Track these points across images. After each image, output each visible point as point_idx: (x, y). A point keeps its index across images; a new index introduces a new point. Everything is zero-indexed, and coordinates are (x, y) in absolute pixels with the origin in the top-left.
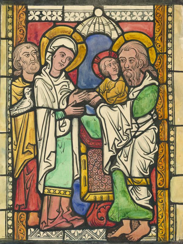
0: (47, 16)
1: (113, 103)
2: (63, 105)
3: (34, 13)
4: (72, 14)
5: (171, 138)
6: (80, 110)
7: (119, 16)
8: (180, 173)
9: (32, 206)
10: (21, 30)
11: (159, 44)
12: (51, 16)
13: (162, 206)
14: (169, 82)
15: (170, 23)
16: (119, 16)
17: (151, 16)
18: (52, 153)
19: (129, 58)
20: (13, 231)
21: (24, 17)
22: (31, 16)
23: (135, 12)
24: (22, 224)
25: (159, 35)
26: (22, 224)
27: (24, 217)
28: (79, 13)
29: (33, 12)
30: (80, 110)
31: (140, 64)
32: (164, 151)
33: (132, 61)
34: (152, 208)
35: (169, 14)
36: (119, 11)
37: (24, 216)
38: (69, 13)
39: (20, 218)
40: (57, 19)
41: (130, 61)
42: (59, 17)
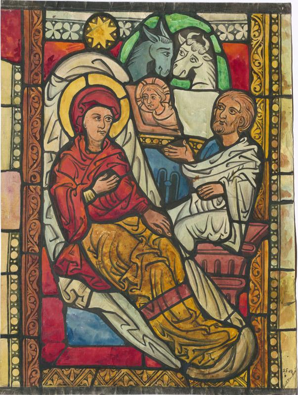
1: (237, 371)
3: (70, 25)
4: (59, 26)
5: (130, 27)
7: (238, 31)
9: (253, 173)
11: (258, 61)
13: (260, 71)
15: (18, 94)
17: (49, 30)
20: (271, 215)
22: (69, 26)
24: (257, 75)
25: (33, 116)
26: (257, 75)
27: (254, 33)
28: (54, 23)
29: (68, 24)
31: (29, 308)
34: (138, 32)
35: (273, 70)
37: (255, 88)
38: (54, 23)
39: (261, 30)
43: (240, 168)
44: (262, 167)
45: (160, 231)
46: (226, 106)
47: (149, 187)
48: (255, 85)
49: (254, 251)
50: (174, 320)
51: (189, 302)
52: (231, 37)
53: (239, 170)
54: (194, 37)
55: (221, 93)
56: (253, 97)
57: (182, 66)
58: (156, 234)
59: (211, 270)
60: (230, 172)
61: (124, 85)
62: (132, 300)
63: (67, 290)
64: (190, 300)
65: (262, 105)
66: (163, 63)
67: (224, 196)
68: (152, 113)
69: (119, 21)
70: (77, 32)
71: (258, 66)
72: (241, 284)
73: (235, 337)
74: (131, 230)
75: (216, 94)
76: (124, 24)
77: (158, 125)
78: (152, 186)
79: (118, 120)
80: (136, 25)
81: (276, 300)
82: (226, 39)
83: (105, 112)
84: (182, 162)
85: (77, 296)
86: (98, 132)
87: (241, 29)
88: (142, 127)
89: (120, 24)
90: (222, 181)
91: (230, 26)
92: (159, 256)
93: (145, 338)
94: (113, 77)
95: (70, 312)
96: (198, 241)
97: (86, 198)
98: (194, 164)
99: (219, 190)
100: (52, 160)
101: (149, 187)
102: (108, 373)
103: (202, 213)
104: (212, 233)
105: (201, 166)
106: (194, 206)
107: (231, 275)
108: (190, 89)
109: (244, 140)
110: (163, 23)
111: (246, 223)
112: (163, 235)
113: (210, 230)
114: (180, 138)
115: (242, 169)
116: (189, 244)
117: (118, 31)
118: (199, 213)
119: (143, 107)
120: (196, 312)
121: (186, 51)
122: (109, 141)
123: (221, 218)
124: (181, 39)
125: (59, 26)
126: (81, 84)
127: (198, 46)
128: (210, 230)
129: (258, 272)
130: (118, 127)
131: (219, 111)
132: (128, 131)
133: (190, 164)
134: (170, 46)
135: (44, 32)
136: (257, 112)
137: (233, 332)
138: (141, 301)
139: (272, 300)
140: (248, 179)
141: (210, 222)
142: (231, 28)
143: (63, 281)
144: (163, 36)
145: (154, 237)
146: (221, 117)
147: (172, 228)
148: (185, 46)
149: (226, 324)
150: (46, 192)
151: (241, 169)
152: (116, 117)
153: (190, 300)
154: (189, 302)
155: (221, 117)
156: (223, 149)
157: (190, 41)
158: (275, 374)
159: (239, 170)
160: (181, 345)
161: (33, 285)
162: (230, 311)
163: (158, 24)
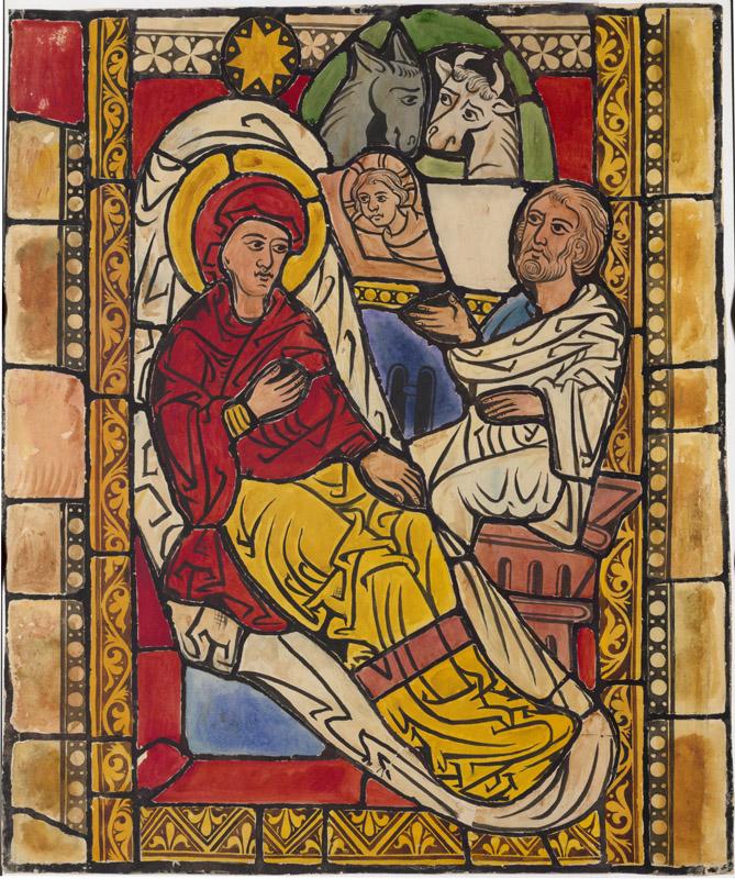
0: (192, 55)
2: (377, 413)
6: (293, 385)
7: (567, 50)
8: (683, 714)
10: (622, 127)
12: (558, 52)
14: (655, 324)
16: (567, 50)
17: (142, 53)
18: (148, 489)
19: (554, 220)
21: (123, 62)
23: (145, 38)
28: (542, 39)
30: (293, 385)
32: (104, 378)
33: (562, 231)
36: (210, 38)
40: (190, 69)
41: (558, 227)
42: (550, 56)
43: (579, 358)
44: (625, 350)
45: (400, 498)
46: (544, 215)
47: (373, 407)
48: (609, 168)
49: (604, 547)
50: (431, 697)
51: (467, 658)
52: (553, 63)
53: (574, 364)
54: (469, 65)
55: (533, 190)
56: (606, 201)
57: (449, 126)
58: (391, 501)
59: (518, 580)
60: (558, 367)
61: (313, 174)
62: (336, 649)
63: (195, 634)
64: (469, 652)
65: (625, 213)
66: (403, 123)
67: (547, 420)
68: (382, 234)
69: (299, 31)
70: (207, 57)
71: (619, 130)
72: (584, 616)
73: (565, 736)
74: (328, 498)
75: (519, 194)
76: (313, 37)
77: (396, 259)
78: (377, 402)
79: (301, 250)
80: (339, 39)
81: (659, 60)
82: (527, 51)
83: (273, 233)
84: (447, 343)
85: (213, 645)
86: (256, 275)
87: (574, 54)
88: (358, 266)
89: (303, 37)
90: (538, 386)
91: (550, 39)
92: (393, 553)
93: (366, 739)
94: (294, 157)
95: (197, 679)
96: (480, 519)
97: (432, 309)
98: (471, 348)
99: (533, 407)
100: (151, 346)
101: (373, 407)
102: (286, 816)
103: (489, 457)
104: (516, 501)
105: (493, 351)
106: (473, 440)
107: (564, 596)
108: (465, 182)
109: (588, 290)
110: (401, 38)
111: (591, 482)
112: (407, 505)
113: (511, 493)
114: (447, 292)
115: (583, 359)
116: (463, 525)
117: (296, 53)
118: (483, 458)
119: (364, 223)
120: (480, 678)
121: (455, 94)
122: (286, 303)
123: (531, 468)
124: (441, 67)
125: (165, 44)
126: (219, 168)
127: (479, 82)
128: (511, 493)
129: (624, 584)
130: (297, 267)
131: (531, 230)
132: (326, 274)
133: (465, 346)
134: (416, 81)
135: (131, 58)
136: (124, 798)
137: (561, 724)
138: (354, 651)
139: (653, 756)
140: (599, 384)
141: (513, 483)
142: (551, 44)
143: (182, 615)
144: (506, 114)
145: (383, 507)
146: (538, 240)
147: (426, 491)
148: (451, 84)
149: (545, 706)
150: (141, 417)
151: (579, 361)
152: (297, 242)
153: (469, 652)
154: (467, 658)
155: (538, 240)
156: (540, 316)
157: (461, 72)
158: (655, 109)
159: (574, 364)
160: (446, 756)
161: (117, 622)
162: (560, 675)
163: (390, 35)
